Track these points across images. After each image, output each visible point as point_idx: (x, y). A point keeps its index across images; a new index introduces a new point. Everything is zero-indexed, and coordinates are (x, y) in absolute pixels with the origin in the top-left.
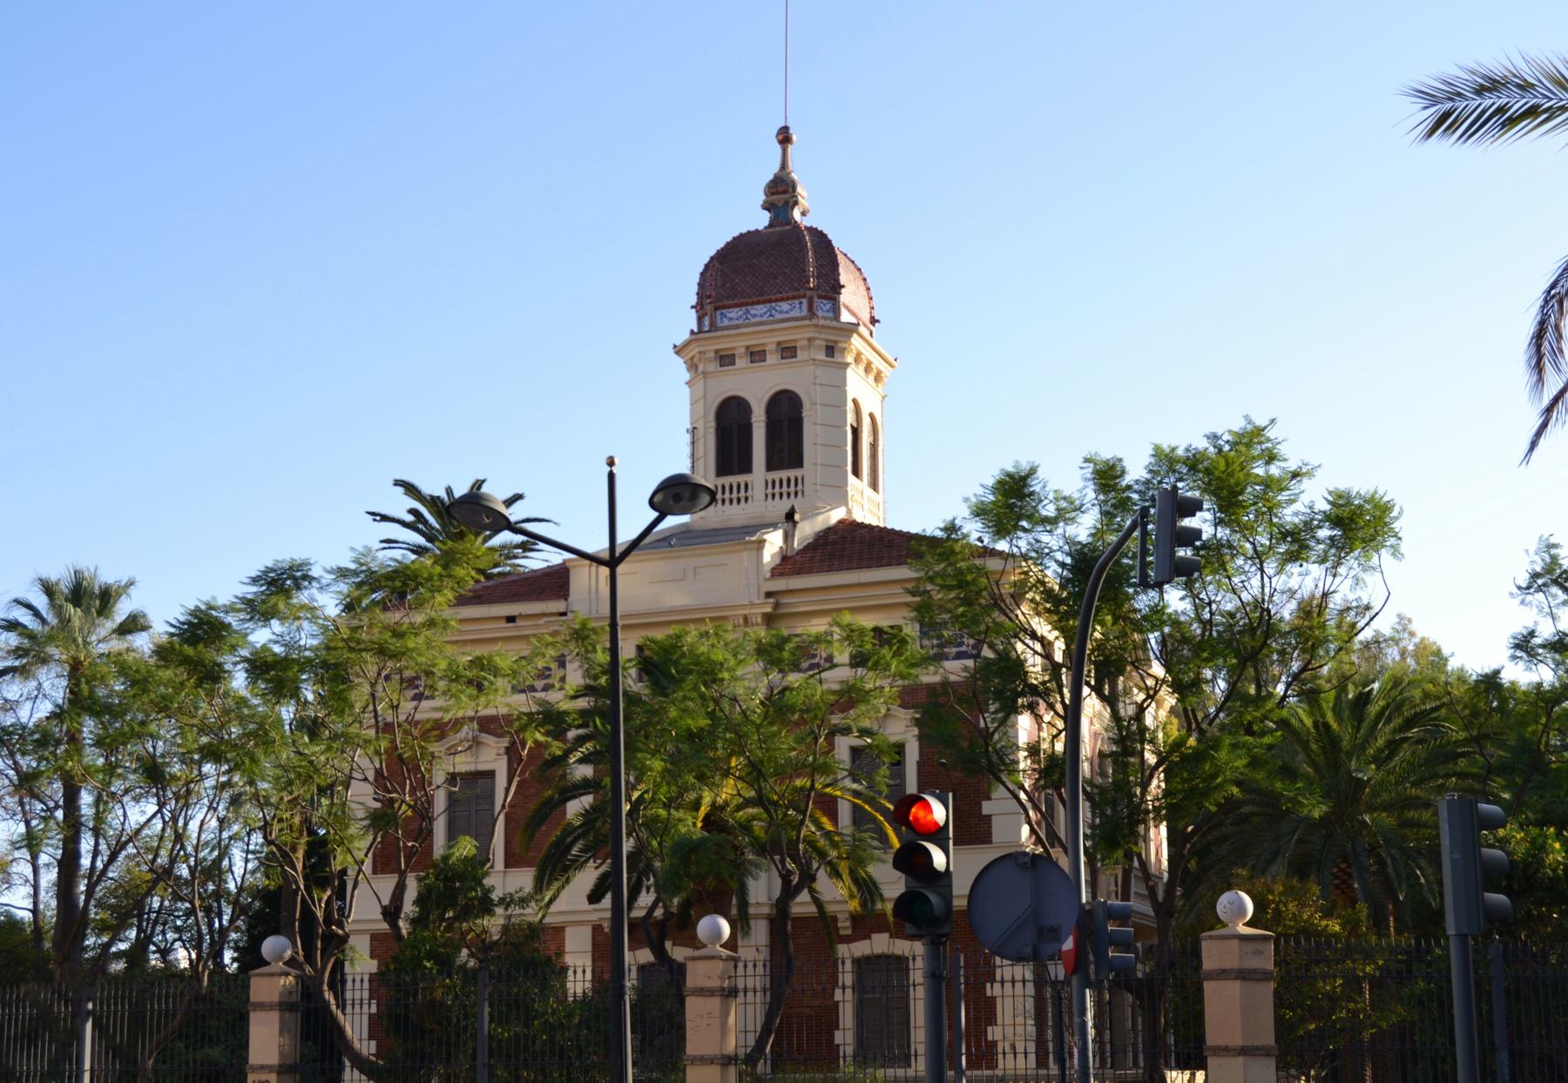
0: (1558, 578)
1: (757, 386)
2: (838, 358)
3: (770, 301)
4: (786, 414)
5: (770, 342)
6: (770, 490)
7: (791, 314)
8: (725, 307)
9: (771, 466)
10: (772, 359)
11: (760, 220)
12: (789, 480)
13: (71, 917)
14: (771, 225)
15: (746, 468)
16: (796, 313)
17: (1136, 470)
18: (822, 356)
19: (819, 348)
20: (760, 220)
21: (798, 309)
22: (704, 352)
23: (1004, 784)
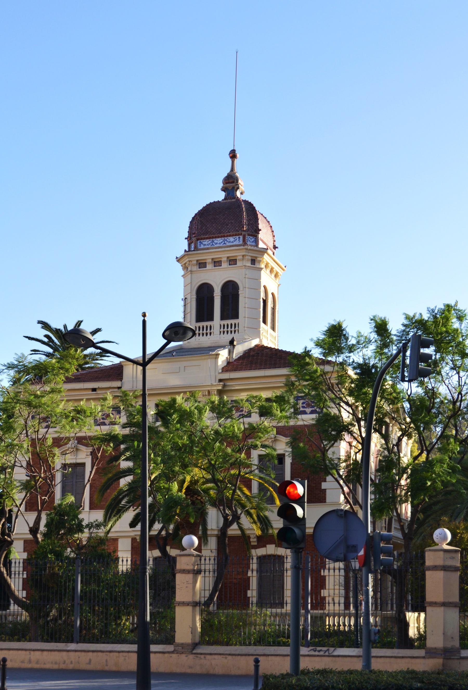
1: (217, 278)
2: (257, 265)
3: (224, 236)
4: (231, 291)
5: (224, 256)
6: (222, 329)
7: (234, 243)
8: (202, 239)
10: (225, 265)
11: (220, 196)
14: (225, 199)
15: (211, 318)
16: (237, 243)
18: (249, 264)
19: (248, 260)
20: (220, 196)
21: (238, 240)
22: (191, 261)
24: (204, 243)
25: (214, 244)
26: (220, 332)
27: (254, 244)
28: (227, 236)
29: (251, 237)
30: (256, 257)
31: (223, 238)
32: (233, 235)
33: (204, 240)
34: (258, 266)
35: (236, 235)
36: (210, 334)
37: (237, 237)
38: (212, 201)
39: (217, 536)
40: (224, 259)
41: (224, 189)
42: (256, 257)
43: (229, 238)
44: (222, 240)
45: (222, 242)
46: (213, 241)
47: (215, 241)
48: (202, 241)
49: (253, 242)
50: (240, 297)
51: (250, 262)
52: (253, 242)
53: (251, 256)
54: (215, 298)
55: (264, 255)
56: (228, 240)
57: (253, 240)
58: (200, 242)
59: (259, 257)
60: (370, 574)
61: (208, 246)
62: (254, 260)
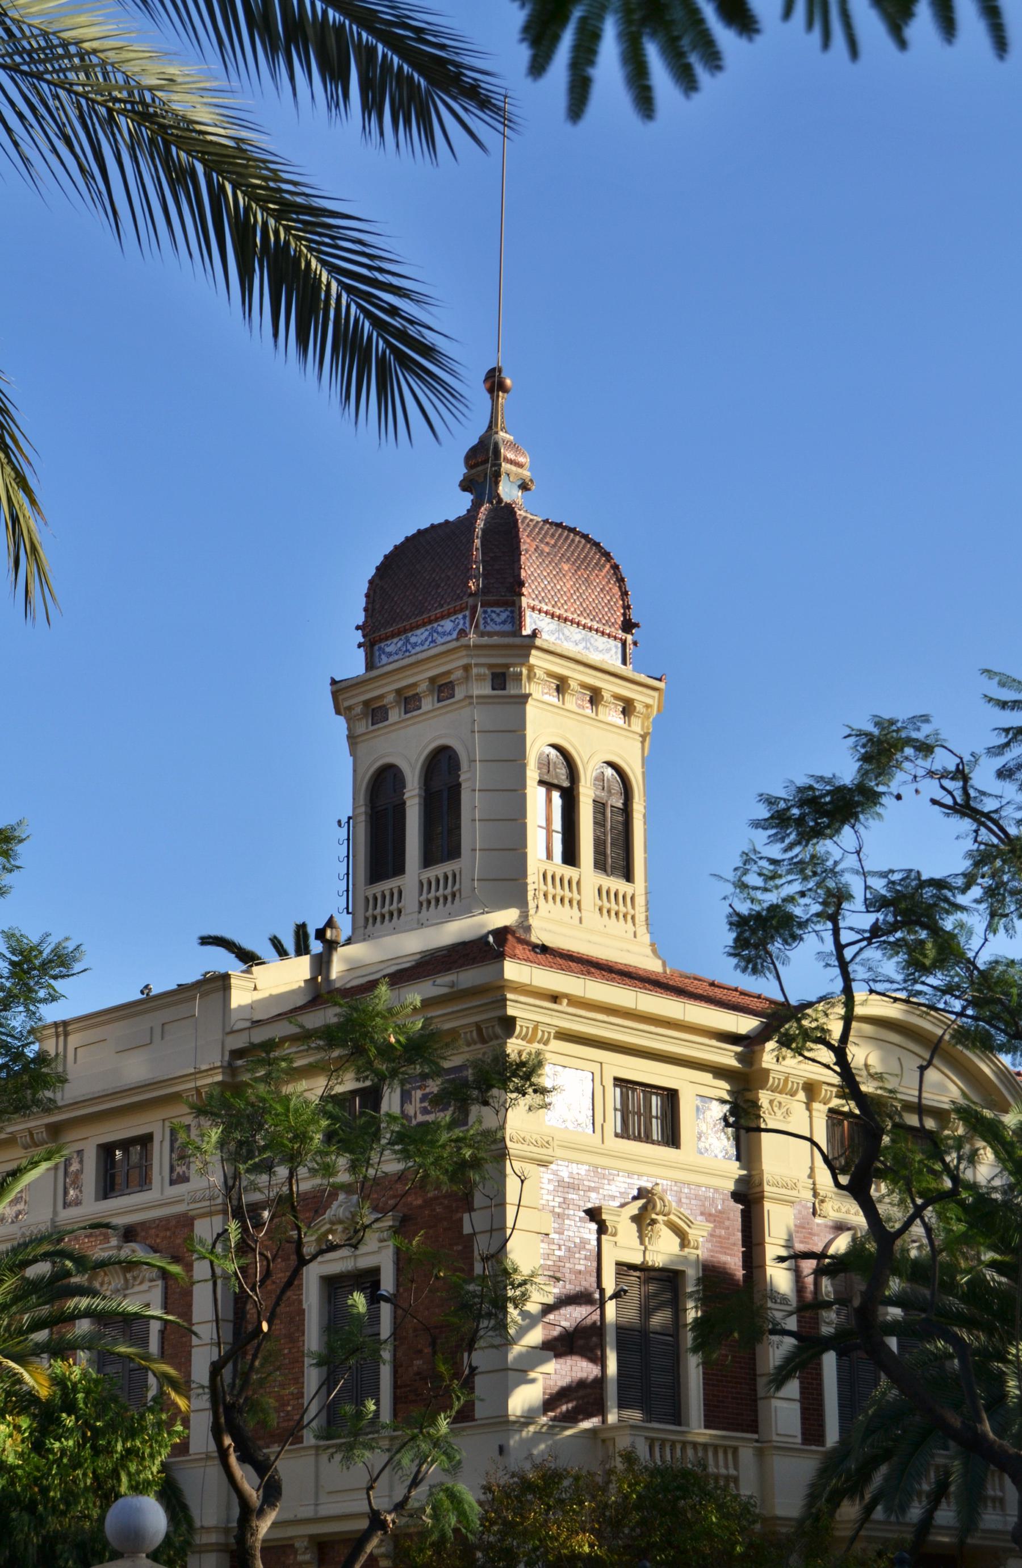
0: (788, 11)
2: (512, 690)
3: (430, 622)
8: (381, 640)
9: (428, 861)
11: (456, 505)
12: (446, 878)
13: (935, 1252)
15: (399, 869)
17: (362, 640)
18: (486, 690)
19: (480, 678)
22: (361, 707)
23: (317, 1462)
24: (388, 650)
25: (409, 647)
26: (421, 904)
27: (508, 627)
28: (437, 620)
29: (498, 610)
30: (507, 666)
31: (429, 627)
32: (449, 615)
33: (389, 642)
34: (513, 692)
35: (455, 613)
36: (400, 912)
37: (460, 616)
38: (424, 525)
39: (221, 1548)
40: (423, 687)
41: (466, 485)
42: (507, 666)
43: (442, 623)
44: (427, 633)
45: (426, 639)
46: (408, 640)
47: (413, 640)
48: (382, 645)
49: (504, 622)
50: (463, 792)
51: (488, 684)
52: (504, 622)
53: (490, 666)
54: (408, 803)
55: (528, 655)
56: (440, 629)
57: (504, 616)
58: (380, 648)
59: (514, 665)
60: (931, 1538)
61: (396, 657)
62: (504, 675)
